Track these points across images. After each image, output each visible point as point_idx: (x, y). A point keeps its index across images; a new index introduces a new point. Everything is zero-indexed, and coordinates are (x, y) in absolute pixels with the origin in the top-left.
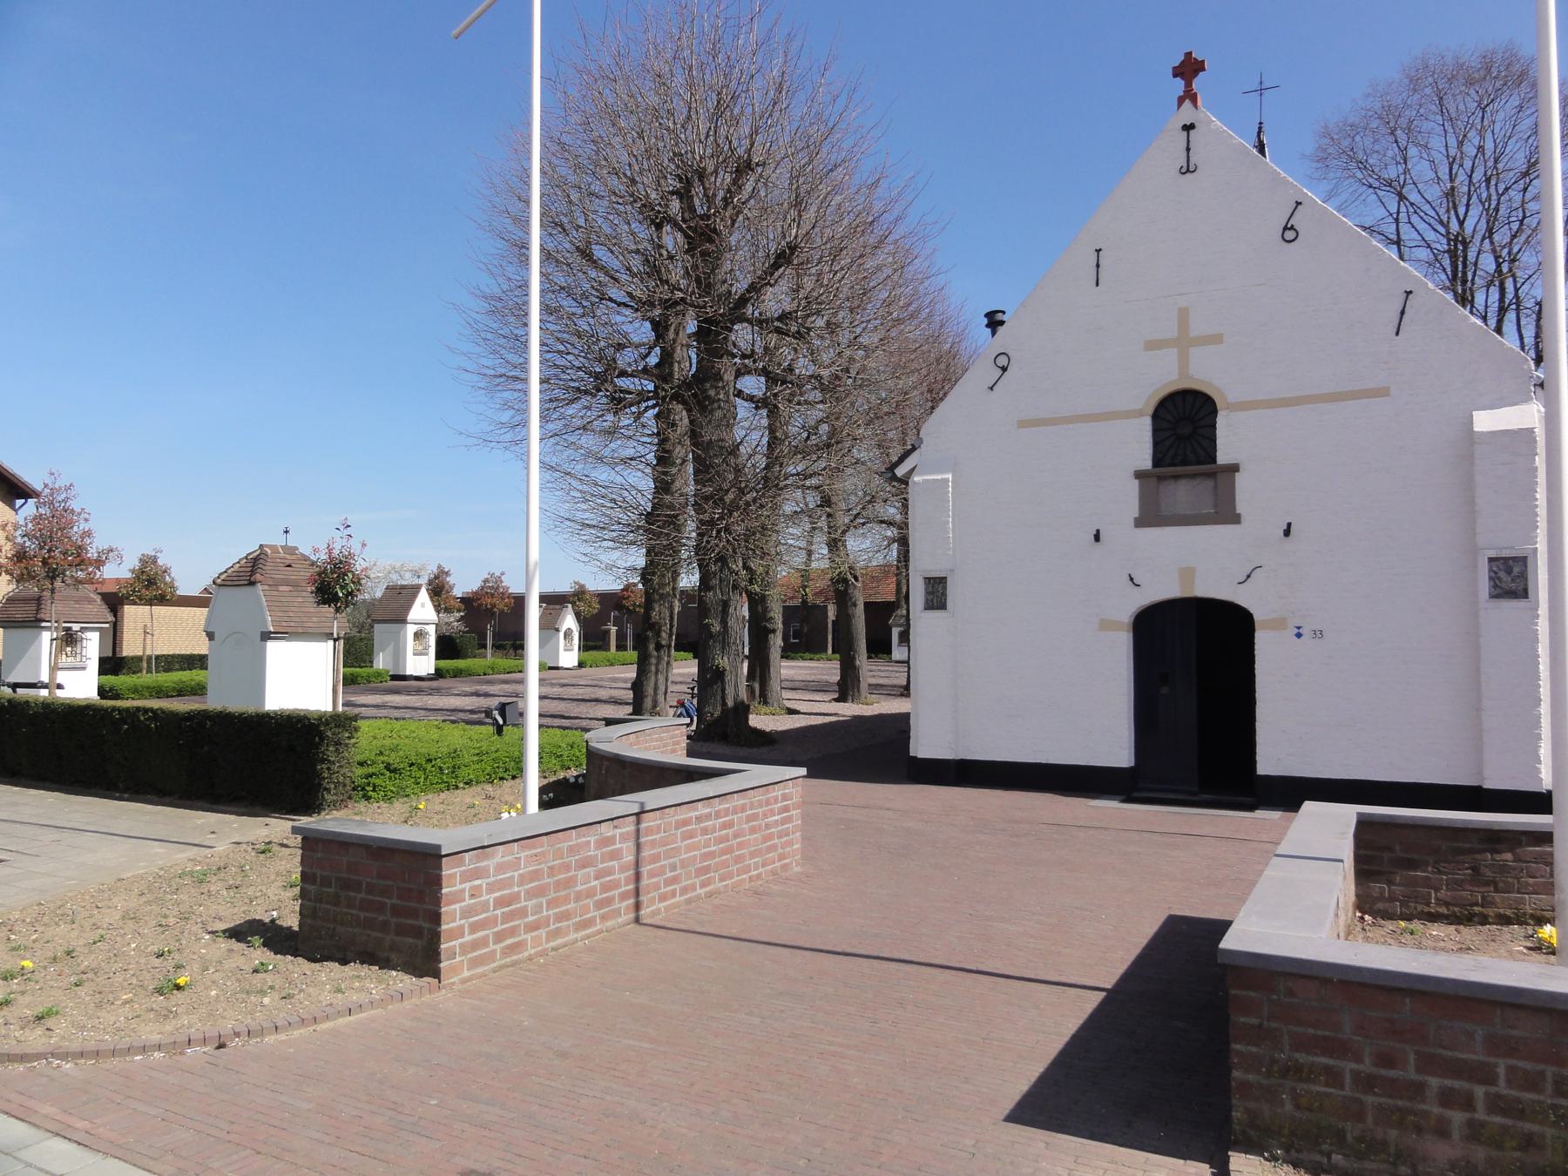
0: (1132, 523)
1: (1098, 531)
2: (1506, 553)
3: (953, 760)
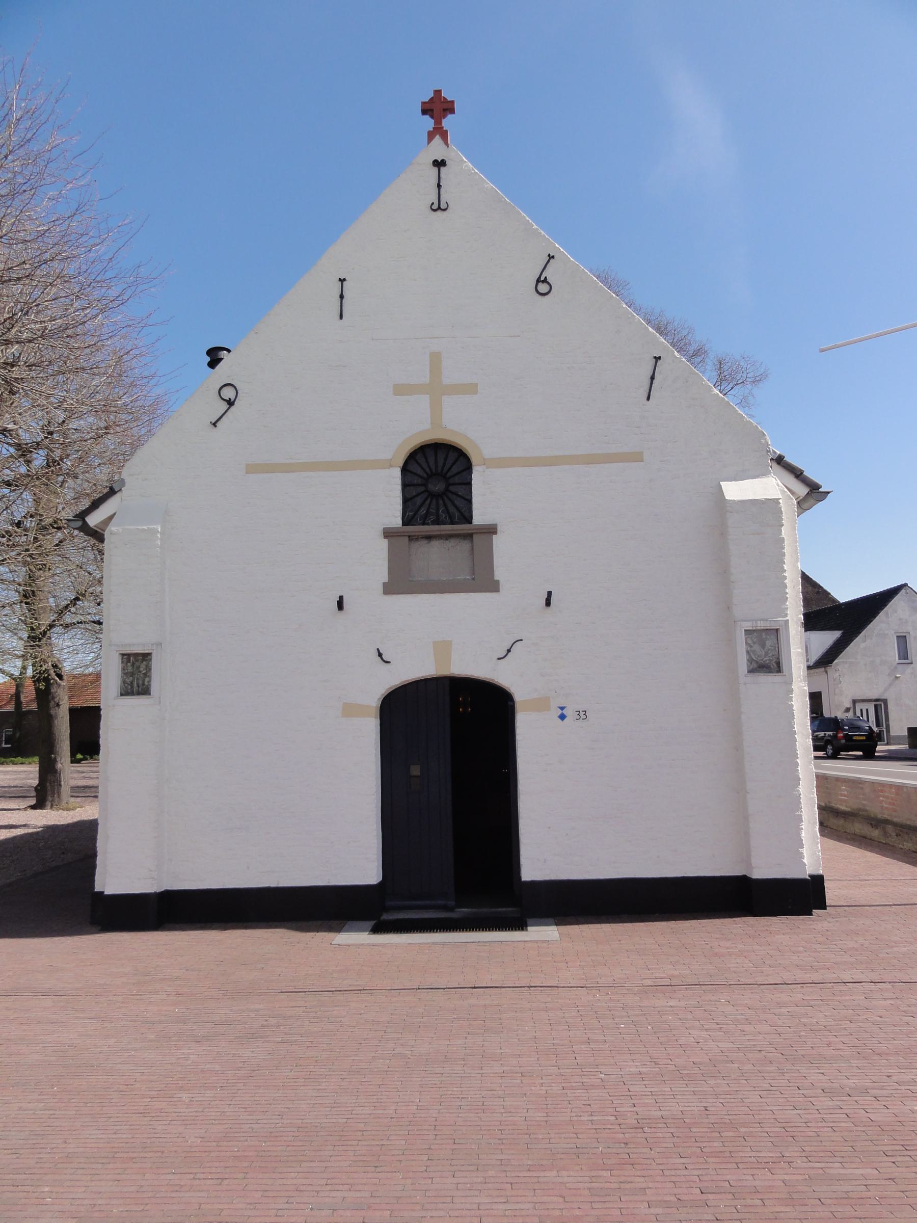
0: (381, 588)
1: (341, 598)
2: (761, 625)
3: (155, 894)
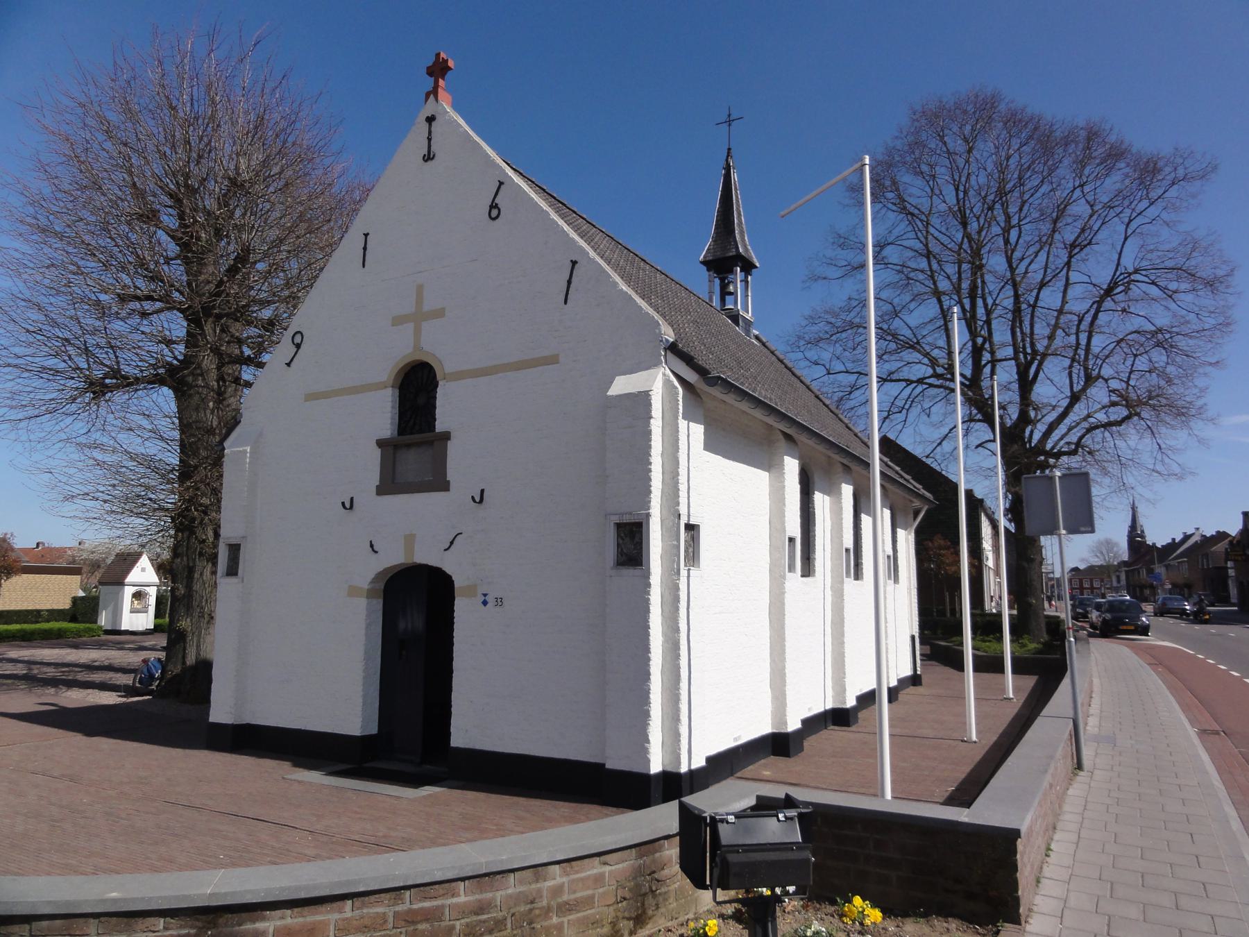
0: (374, 489)
